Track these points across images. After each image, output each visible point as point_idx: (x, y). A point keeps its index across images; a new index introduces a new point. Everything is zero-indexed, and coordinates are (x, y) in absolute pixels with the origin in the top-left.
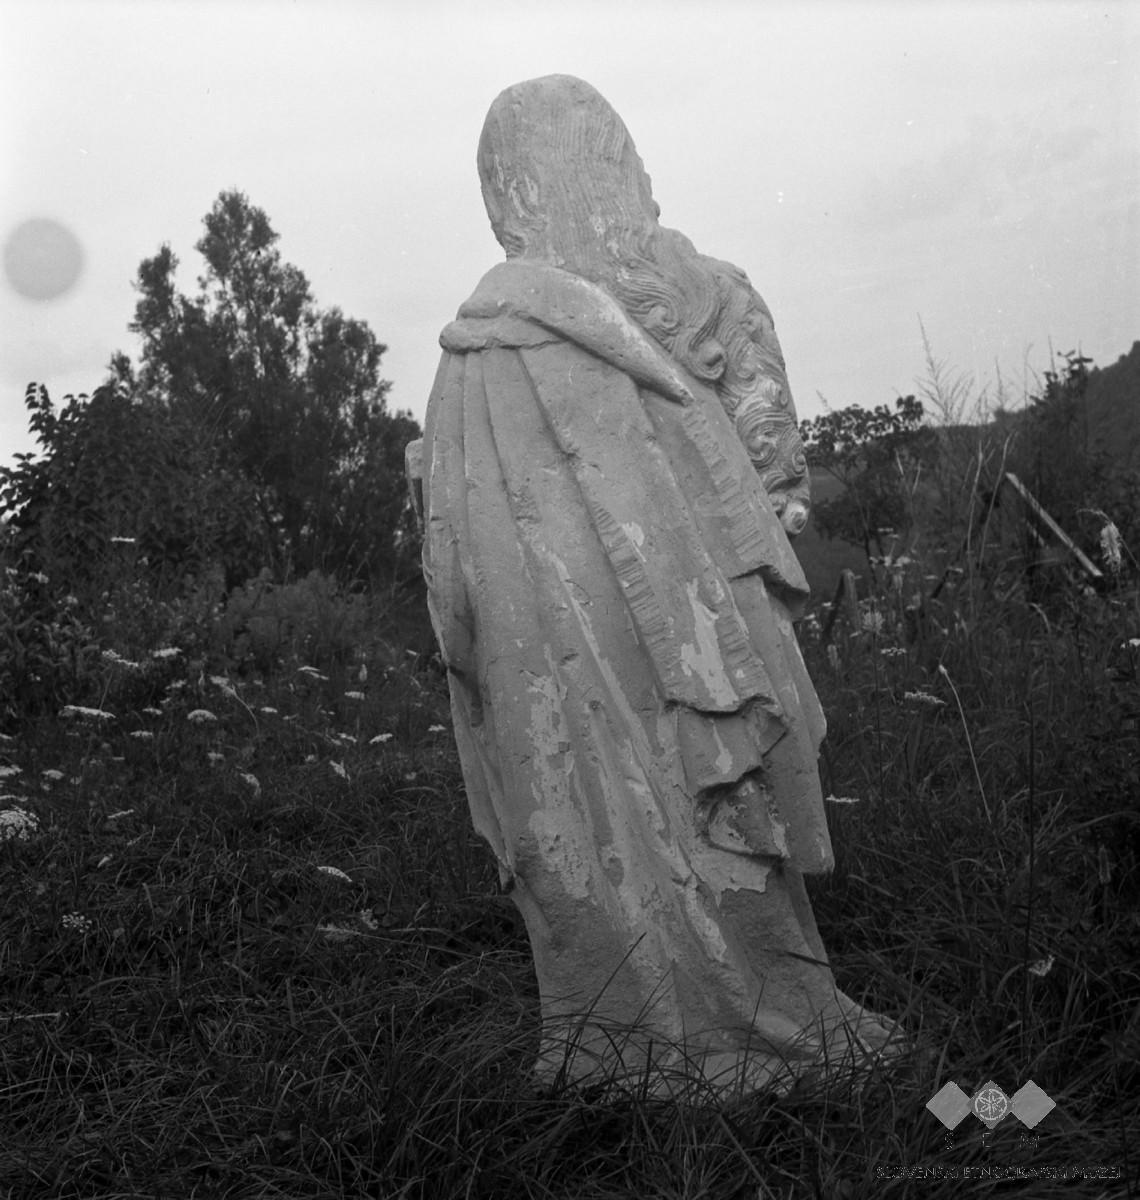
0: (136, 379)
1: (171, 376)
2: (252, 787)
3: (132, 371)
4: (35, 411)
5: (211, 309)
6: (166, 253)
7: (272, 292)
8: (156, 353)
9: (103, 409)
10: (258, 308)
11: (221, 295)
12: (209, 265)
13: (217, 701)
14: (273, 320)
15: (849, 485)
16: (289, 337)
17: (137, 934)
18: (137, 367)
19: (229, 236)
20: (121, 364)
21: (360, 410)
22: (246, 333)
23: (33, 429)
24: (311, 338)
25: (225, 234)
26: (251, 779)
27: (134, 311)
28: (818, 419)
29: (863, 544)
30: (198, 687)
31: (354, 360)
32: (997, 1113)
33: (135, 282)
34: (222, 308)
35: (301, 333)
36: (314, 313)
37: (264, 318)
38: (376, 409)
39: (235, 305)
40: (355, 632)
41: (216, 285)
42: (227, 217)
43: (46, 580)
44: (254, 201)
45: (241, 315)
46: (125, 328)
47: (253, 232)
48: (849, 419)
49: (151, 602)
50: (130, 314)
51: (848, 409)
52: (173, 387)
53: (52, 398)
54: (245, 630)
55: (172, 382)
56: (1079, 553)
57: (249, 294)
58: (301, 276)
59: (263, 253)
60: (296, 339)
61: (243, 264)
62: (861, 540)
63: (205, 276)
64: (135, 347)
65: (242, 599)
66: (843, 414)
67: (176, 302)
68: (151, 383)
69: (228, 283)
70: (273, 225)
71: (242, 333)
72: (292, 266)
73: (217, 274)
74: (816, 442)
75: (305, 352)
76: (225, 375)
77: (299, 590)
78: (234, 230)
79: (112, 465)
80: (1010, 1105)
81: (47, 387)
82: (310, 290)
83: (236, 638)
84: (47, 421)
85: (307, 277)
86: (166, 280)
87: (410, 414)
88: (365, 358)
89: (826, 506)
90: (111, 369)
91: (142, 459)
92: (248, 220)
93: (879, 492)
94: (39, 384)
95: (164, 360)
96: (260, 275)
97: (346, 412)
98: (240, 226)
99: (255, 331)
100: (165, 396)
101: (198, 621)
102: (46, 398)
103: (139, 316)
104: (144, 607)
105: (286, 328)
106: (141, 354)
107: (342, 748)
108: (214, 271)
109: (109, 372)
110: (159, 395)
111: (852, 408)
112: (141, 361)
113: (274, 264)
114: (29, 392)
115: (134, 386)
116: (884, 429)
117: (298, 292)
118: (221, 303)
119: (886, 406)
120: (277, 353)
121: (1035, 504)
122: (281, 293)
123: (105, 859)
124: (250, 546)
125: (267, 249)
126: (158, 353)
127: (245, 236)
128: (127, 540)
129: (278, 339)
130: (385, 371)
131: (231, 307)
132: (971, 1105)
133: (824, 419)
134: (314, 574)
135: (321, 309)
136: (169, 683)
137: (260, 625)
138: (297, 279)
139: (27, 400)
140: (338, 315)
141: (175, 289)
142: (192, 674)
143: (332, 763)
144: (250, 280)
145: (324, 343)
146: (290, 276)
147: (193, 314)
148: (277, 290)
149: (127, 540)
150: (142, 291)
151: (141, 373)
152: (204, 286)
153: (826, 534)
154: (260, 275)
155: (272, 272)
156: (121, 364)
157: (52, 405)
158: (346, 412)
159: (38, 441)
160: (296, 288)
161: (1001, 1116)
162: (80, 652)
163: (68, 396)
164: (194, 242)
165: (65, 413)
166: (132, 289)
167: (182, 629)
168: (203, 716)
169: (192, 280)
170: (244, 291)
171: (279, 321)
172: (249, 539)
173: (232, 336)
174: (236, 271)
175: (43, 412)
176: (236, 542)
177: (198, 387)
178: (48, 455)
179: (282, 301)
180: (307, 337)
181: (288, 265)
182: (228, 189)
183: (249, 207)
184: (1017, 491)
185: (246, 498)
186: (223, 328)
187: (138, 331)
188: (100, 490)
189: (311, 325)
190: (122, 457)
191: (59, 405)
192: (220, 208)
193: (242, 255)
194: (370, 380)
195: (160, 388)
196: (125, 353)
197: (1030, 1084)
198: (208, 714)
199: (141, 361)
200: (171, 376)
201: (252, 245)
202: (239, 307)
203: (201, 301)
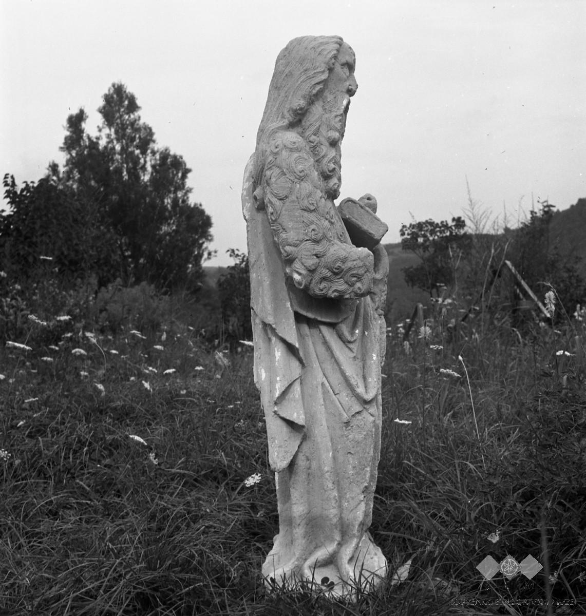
0: (61, 175)
1: (79, 176)
4: (7, 188)
5: (103, 143)
7: (135, 137)
10: (127, 144)
11: (108, 136)
14: (134, 151)
16: (142, 161)
18: (62, 169)
19: (115, 106)
23: (6, 197)
24: (153, 162)
27: (63, 141)
34: (108, 143)
35: (148, 159)
36: (156, 149)
37: (130, 150)
39: (115, 142)
41: (106, 131)
42: (115, 96)
43: (6, 275)
44: (130, 89)
45: (118, 147)
46: (57, 149)
47: (128, 105)
48: (427, 226)
50: (61, 142)
51: (427, 221)
52: (80, 181)
54: (106, 310)
58: (150, 129)
59: (132, 116)
60: (145, 162)
61: (121, 121)
63: (101, 126)
64: (61, 159)
65: (105, 294)
66: (424, 223)
67: (85, 138)
69: (113, 130)
70: (139, 102)
72: (146, 124)
73: (107, 125)
74: (409, 237)
82: (155, 137)
85: (154, 130)
89: (411, 270)
90: (48, 169)
92: (126, 99)
94: (11, 175)
96: (129, 127)
99: (124, 156)
102: (13, 182)
103: (65, 143)
104: (54, 293)
107: (149, 375)
108: (106, 123)
111: (429, 221)
112: (64, 166)
113: (137, 122)
115: (59, 179)
116: (444, 233)
117: (149, 138)
118: (108, 140)
119: (446, 221)
120: (135, 168)
125: (134, 114)
129: (136, 161)
132: (499, 567)
135: (160, 147)
137: (112, 307)
138: (148, 131)
140: (168, 151)
141: (85, 131)
144: (124, 129)
145: (160, 165)
147: (93, 145)
148: (137, 136)
150: (68, 130)
152: (100, 130)
154: (129, 127)
156: (54, 168)
157: (16, 186)
160: (147, 136)
163: (25, 182)
165: (22, 190)
166: (63, 129)
168: (80, 352)
173: (112, 158)
174: (117, 124)
175: (11, 189)
178: (12, 211)
180: (151, 161)
181: (144, 123)
182: (117, 81)
187: (64, 151)
190: (50, 215)
191: (20, 186)
192: (112, 91)
193: (121, 116)
196: (56, 162)
198: (82, 351)
200: (79, 176)
201: (126, 111)
202: (117, 143)
203: (98, 138)
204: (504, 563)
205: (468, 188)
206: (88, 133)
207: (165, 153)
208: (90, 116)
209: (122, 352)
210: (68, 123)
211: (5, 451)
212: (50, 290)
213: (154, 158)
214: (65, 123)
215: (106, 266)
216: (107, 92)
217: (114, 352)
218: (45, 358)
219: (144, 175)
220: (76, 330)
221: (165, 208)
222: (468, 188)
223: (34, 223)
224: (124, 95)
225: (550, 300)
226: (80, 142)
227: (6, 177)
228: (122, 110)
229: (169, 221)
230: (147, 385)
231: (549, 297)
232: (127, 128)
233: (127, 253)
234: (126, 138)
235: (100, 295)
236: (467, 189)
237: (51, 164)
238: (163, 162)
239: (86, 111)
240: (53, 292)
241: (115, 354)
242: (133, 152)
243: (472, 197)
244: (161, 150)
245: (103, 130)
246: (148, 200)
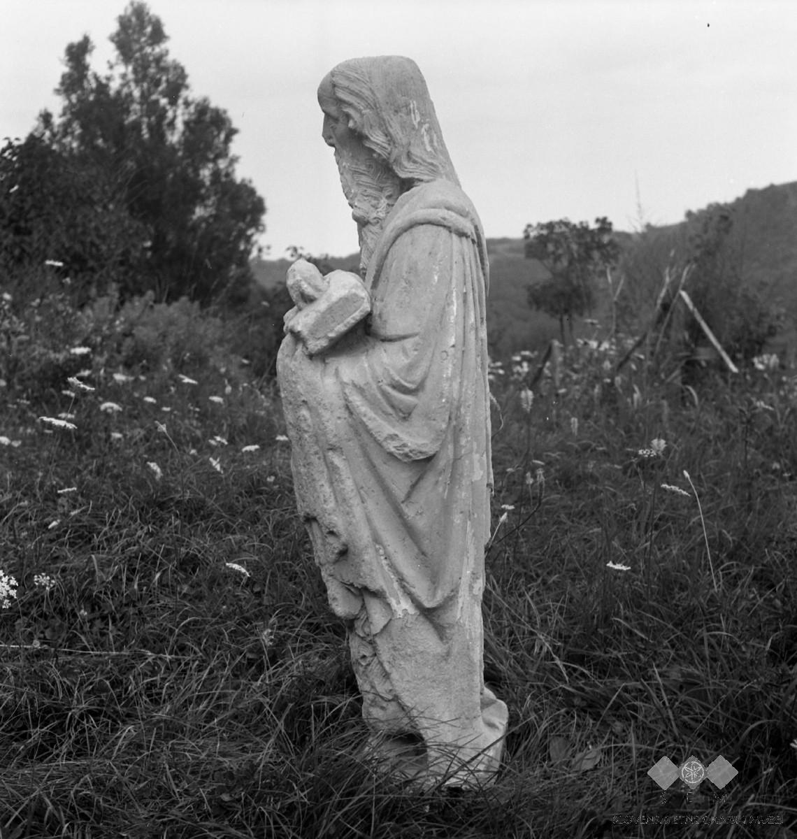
0: (56, 130)
5: (115, 85)
8: (72, 113)
10: (149, 89)
13: (115, 393)
15: (554, 274)
16: (170, 114)
17: (85, 589)
18: (57, 121)
19: (134, 32)
20: (46, 118)
21: (216, 174)
24: (186, 117)
25: (130, 31)
30: (99, 377)
31: (214, 137)
34: (123, 86)
35: (179, 112)
38: (227, 175)
39: (133, 85)
40: (211, 346)
41: (121, 69)
45: (137, 93)
49: (71, 311)
50: (56, 82)
52: (82, 138)
55: (80, 134)
56: (724, 354)
57: (144, 78)
58: (183, 70)
60: (175, 117)
64: (57, 106)
68: (65, 134)
69: (130, 68)
70: (167, 30)
71: (136, 107)
76: (121, 134)
77: (174, 310)
78: (137, 29)
79: (38, 195)
80: (706, 773)
82: (189, 81)
85: (187, 71)
86: (84, 59)
87: (250, 181)
88: (222, 136)
91: (60, 193)
93: (575, 282)
95: (77, 118)
97: (206, 173)
98: (142, 26)
100: (75, 145)
103: (62, 84)
105: (168, 107)
110: (71, 143)
112: (61, 116)
121: (698, 317)
122: (167, 81)
123: (54, 523)
124: (131, 267)
126: (77, 112)
127: (144, 35)
130: (235, 148)
134: (184, 299)
137: (142, 332)
142: (94, 367)
143: (211, 459)
147: (102, 88)
148: (164, 78)
150: (67, 65)
151: (59, 126)
152: (111, 67)
153: (534, 307)
155: (162, 64)
156: (46, 118)
158: (206, 173)
161: (700, 781)
162: (15, 340)
163: (6, 138)
167: (91, 333)
168: (112, 408)
171: (164, 101)
177: (100, 142)
179: (168, 87)
184: (686, 305)
186: (121, 103)
188: (28, 212)
190: (45, 191)
193: (141, 49)
194: (223, 154)
196: (50, 110)
199: (61, 116)
201: (150, 42)
203: (108, 79)
216: (122, 13)
240: (62, 312)
242: (157, 102)
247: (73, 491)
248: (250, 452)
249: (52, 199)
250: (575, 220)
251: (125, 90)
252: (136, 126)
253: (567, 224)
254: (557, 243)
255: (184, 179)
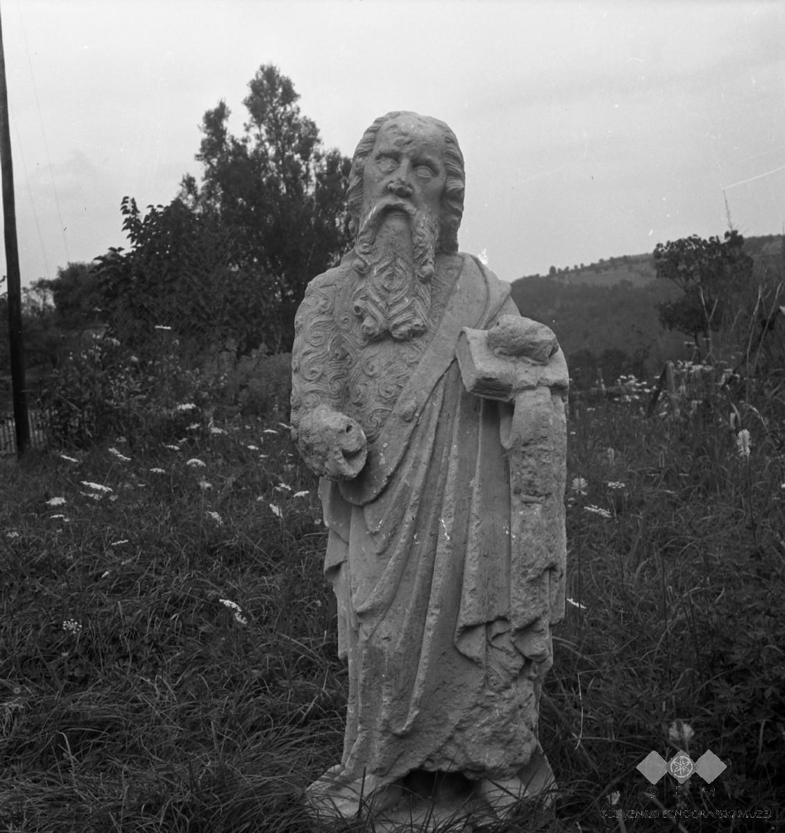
0: (199, 192)
1: (222, 192)
2: (215, 521)
3: (196, 188)
4: (127, 216)
5: (251, 147)
6: (222, 106)
7: (293, 135)
9: (170, 220)
10: (283, 146)
11: (258, 137)
12: (251, 115)
14: (293, 156)
15: (687, 291)
16: (304, 168)
18: (200, 184)
19: (266, 96)
22: (274, 164)
23: (125, 228)
24: (318, 170)
26: (215, 515)
27: (200, 146)
28: (668, 243)
29: (693, 334)
32: (686, 773)
33: (201, 126)
34: (259, 145)
35: (311, 165)
36: (321, 152)
37: (287, 153)
39: (267, 144)
41: (255, 130)
42: (265, 82)
43: (119, 343)
44: (284, 72)
45: (272, 151)
46: (192, 157)
47: (282, 93)
48: (690, 245)
50: (197, 148)
51: (690, 238)
52: (224, 201)
53: (138, 206)
54: (246, 386)
58: (313, 125)
59: (289, 108)
60: (308, 170)
61: (274, 115)
62: (692, 331)
63: (248, 123)
64: (199, 171)
65: (248, 364)
66: (686, 241)
67: (228, 141)
69: (264, 127)
70: (296, 89)
72: (308, 118)
73: (256, 122)
74: (665, 260)
75: (314, 179)
80: (694, 767)
81: (136, 200)
82: (319, 136)
83: (241, 390)
84: (135, 223)
85: (318, 126)
86: (222, 125)
89: (669, 306)
90: (182, 185)
92: (279, 85)
94: (131, 198)
95: (218, 181)
96: (285, 124)
98: (274, 90)
99: (281, 162)
100: (218, 206)
101: (210, 385)
102: (134, 207)
103: (203, 149)
104: (175, 373)
106: (203, 175)
107: (281, 493)
108: (254, 120)
109: (181, 188)
111: (693, 237)
112: (203, 180)
113: (296, 115)
114: (123, 203)
115: (197, 198)
116: (715, 253)
117: (311, 136)
118: (259, 142)
119: (717, 237)
120: (295, 178)
123: (107, 573)
125: (291, 105)
128: (165, 328)
129: (296, 168)
131: (265, 146)
132: (668, 767)
133: (673, 243)
135: (326, 150)
136: (189, 425)
137: (255, 383)
138: (311, 127)
139: (122, 209)
140: (337, 154)
141: (228, 132)
144: (279, 127)
145: (328, 173)
146: (306, 125)
147: (240, 149)
148: (297, 135)
149: (165, 328)
150: (205, 132)
151: (202, 189)
152: (247, 129)
154: (285, 124)
155: (293, 121)
156: (189, 183)
157: (139, 212)
159: (128, 237)
160: (309, 133)
161: (688, 775)
163: (150, 206)
164: (242, 99)
165: (147, 218)
166: (198, 130)
167: (199, 388)
168: (196, 463)
169: (239, 126)
170: (275, 134)
171: (297, 157)
172: (263, 313)
173: (265, 166)
174: (270, 120)
175: (133, 216)
176: (255, 315)
178: (134, 247)
179: (300, 142)
180: (315, 169)
181: (305, 117)
182: (266, 63)
183: (281, 76)
185: (263, 284)
187: (202, 160)
189: (318, 161)
190: (180, 254)
191: (144, 212)
192: (260, 77)
193: (275, 109)
195: (215, 199)
196: (192, 175)
197: (709, 752)
198: (200, 462)
200: (222, 192)
201: (281, 102)
202: (270, 145)
203: (245, 140)
204: (674, 761)
205: (727, 209)
206: (231, 134)
207: (333, 157)
208: (233, 111)
209: (263, 447)
210: (206, 123)
211: (74, 622)
212: (170, 369)
213: (319, 164)
214: (202, 123)
215: (256, 317)
216: (254, 77)
217: (252, 447)
218: (154, 470)
219: (307, 188)
220: (205, 420)
221: (336, 231)
222: (727, 209)
223: (160, 265)
224: (277, 82)
225: (744, 441)
226: (222, 146)
227: (125, 201)
228: (275, 100)
229: (342, 249)
230: (275, 509)
231: (744, 436)
232: (282, 124)
233: (290, 293)
234: (282, 138)
235: (240, 366)
236: (725, 211)
237: (186, 178)
238: (331, 169)
239: (227, 104)
240: (173, 371)
241: (255, 450)
242: (291, 157)
243: (732, 220)
244: (328, 153)
245: (252, 129)
246: (313, 220)
247: (126, 543)
248: (301, 497)
249: (187, 262)
250: (705, 236)
251: (262, 149)
252: (273, 183)
253: (696, 241)
254: (689, 261)
255: (319, 227)
